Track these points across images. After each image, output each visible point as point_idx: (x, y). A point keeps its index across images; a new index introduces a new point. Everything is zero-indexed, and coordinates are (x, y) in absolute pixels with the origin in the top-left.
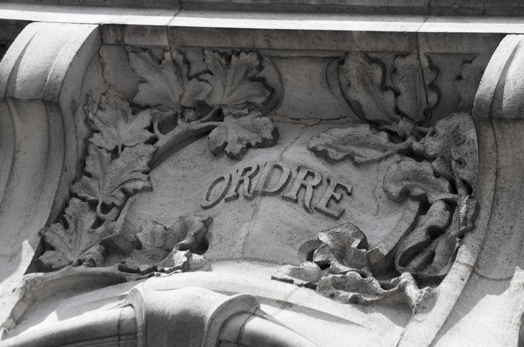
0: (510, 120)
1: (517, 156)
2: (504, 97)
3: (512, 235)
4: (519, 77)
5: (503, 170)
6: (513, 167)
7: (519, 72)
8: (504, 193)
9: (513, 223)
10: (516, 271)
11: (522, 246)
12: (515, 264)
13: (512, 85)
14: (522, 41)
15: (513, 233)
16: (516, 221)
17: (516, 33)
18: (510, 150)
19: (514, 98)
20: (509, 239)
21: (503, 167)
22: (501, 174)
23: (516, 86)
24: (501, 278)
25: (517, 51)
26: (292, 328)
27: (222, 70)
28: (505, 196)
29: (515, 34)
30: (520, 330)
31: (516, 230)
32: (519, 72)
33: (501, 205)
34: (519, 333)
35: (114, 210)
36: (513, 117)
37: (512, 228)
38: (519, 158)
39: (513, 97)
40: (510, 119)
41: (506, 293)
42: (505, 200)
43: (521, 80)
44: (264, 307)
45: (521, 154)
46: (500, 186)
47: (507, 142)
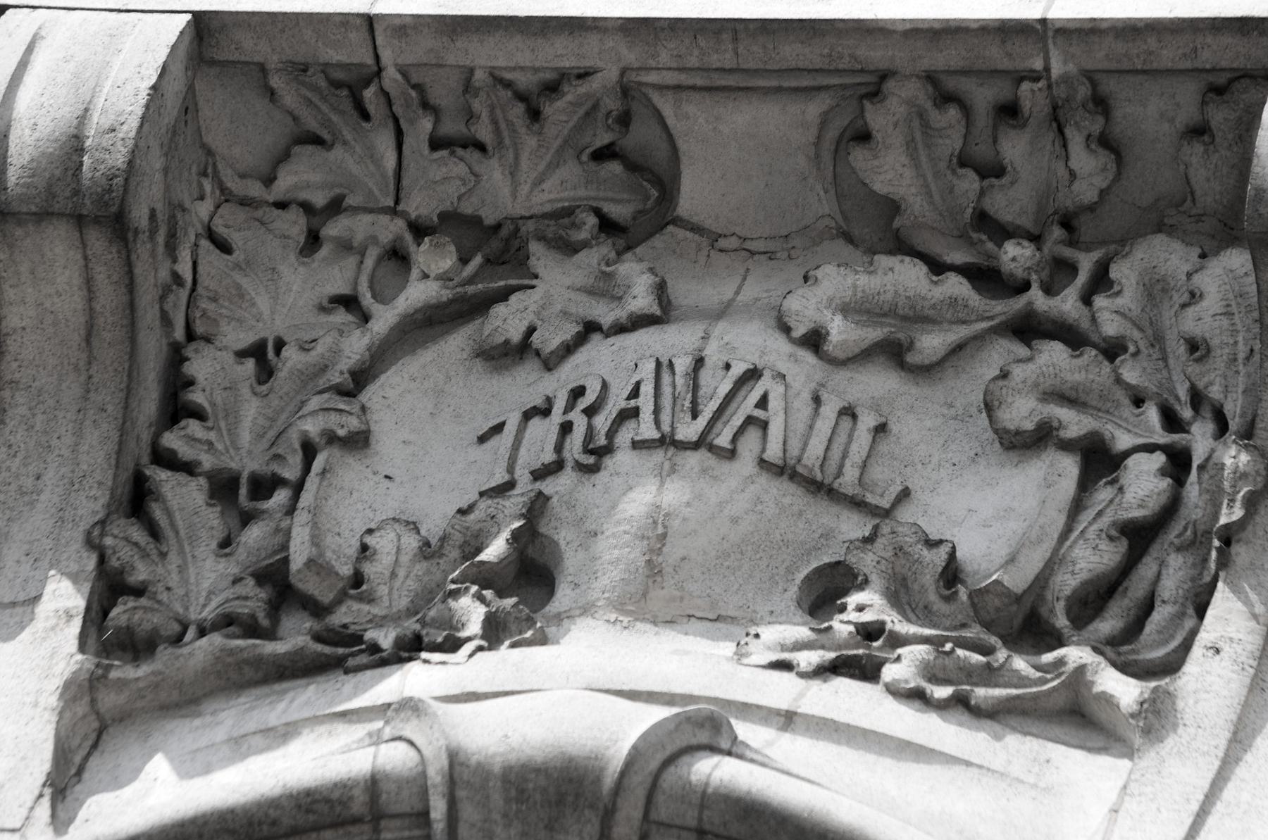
0: (28, 217)
1: (48, 305)
2: (9, 160)
3: (38, 495)
4: (44, 111)
5: (13, 337)
6: (39, 331)
7: (43, 99)
8: (17, 393)
9: (42, 466)
10: (49, 580)
11: (63, 521)
12: (46, 563)
13: (27, 132)
14: (47, 25)
15: (42, 491)
16: (49, 460)
17: (31, 4)
18: (30, 290)
19: (35, 164)
20: (32, 504)
21: (15, 331)
22: (10, 348)
23: (37, 135)
24: (12, 599)
25: (36, 50)
26: (812, 778)
27: (1047, 158)
28: (21, 401)
29: (27, 7)
30: (58, 722)
31: (49, 483)
32: (43, 99)
33: (11, 424)
34: (56, 729)
35: (281, 497)
36: (34, 209)
37: (38, 478)
38: (53, 309)
39: (32, 160)
40: (27, 214)
41: (25, 635)
42: (22, 410)
43: (49, 119)
44: (745, 730)
45: (56, 300)
46: (8, 377)
47: (22, 269)
